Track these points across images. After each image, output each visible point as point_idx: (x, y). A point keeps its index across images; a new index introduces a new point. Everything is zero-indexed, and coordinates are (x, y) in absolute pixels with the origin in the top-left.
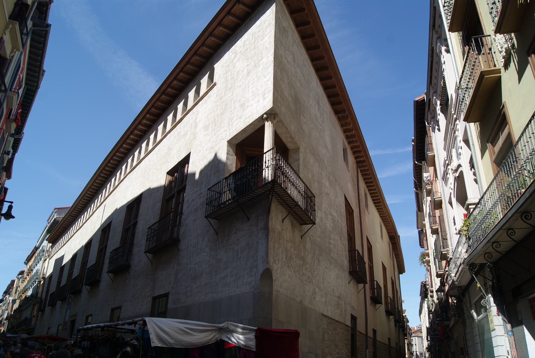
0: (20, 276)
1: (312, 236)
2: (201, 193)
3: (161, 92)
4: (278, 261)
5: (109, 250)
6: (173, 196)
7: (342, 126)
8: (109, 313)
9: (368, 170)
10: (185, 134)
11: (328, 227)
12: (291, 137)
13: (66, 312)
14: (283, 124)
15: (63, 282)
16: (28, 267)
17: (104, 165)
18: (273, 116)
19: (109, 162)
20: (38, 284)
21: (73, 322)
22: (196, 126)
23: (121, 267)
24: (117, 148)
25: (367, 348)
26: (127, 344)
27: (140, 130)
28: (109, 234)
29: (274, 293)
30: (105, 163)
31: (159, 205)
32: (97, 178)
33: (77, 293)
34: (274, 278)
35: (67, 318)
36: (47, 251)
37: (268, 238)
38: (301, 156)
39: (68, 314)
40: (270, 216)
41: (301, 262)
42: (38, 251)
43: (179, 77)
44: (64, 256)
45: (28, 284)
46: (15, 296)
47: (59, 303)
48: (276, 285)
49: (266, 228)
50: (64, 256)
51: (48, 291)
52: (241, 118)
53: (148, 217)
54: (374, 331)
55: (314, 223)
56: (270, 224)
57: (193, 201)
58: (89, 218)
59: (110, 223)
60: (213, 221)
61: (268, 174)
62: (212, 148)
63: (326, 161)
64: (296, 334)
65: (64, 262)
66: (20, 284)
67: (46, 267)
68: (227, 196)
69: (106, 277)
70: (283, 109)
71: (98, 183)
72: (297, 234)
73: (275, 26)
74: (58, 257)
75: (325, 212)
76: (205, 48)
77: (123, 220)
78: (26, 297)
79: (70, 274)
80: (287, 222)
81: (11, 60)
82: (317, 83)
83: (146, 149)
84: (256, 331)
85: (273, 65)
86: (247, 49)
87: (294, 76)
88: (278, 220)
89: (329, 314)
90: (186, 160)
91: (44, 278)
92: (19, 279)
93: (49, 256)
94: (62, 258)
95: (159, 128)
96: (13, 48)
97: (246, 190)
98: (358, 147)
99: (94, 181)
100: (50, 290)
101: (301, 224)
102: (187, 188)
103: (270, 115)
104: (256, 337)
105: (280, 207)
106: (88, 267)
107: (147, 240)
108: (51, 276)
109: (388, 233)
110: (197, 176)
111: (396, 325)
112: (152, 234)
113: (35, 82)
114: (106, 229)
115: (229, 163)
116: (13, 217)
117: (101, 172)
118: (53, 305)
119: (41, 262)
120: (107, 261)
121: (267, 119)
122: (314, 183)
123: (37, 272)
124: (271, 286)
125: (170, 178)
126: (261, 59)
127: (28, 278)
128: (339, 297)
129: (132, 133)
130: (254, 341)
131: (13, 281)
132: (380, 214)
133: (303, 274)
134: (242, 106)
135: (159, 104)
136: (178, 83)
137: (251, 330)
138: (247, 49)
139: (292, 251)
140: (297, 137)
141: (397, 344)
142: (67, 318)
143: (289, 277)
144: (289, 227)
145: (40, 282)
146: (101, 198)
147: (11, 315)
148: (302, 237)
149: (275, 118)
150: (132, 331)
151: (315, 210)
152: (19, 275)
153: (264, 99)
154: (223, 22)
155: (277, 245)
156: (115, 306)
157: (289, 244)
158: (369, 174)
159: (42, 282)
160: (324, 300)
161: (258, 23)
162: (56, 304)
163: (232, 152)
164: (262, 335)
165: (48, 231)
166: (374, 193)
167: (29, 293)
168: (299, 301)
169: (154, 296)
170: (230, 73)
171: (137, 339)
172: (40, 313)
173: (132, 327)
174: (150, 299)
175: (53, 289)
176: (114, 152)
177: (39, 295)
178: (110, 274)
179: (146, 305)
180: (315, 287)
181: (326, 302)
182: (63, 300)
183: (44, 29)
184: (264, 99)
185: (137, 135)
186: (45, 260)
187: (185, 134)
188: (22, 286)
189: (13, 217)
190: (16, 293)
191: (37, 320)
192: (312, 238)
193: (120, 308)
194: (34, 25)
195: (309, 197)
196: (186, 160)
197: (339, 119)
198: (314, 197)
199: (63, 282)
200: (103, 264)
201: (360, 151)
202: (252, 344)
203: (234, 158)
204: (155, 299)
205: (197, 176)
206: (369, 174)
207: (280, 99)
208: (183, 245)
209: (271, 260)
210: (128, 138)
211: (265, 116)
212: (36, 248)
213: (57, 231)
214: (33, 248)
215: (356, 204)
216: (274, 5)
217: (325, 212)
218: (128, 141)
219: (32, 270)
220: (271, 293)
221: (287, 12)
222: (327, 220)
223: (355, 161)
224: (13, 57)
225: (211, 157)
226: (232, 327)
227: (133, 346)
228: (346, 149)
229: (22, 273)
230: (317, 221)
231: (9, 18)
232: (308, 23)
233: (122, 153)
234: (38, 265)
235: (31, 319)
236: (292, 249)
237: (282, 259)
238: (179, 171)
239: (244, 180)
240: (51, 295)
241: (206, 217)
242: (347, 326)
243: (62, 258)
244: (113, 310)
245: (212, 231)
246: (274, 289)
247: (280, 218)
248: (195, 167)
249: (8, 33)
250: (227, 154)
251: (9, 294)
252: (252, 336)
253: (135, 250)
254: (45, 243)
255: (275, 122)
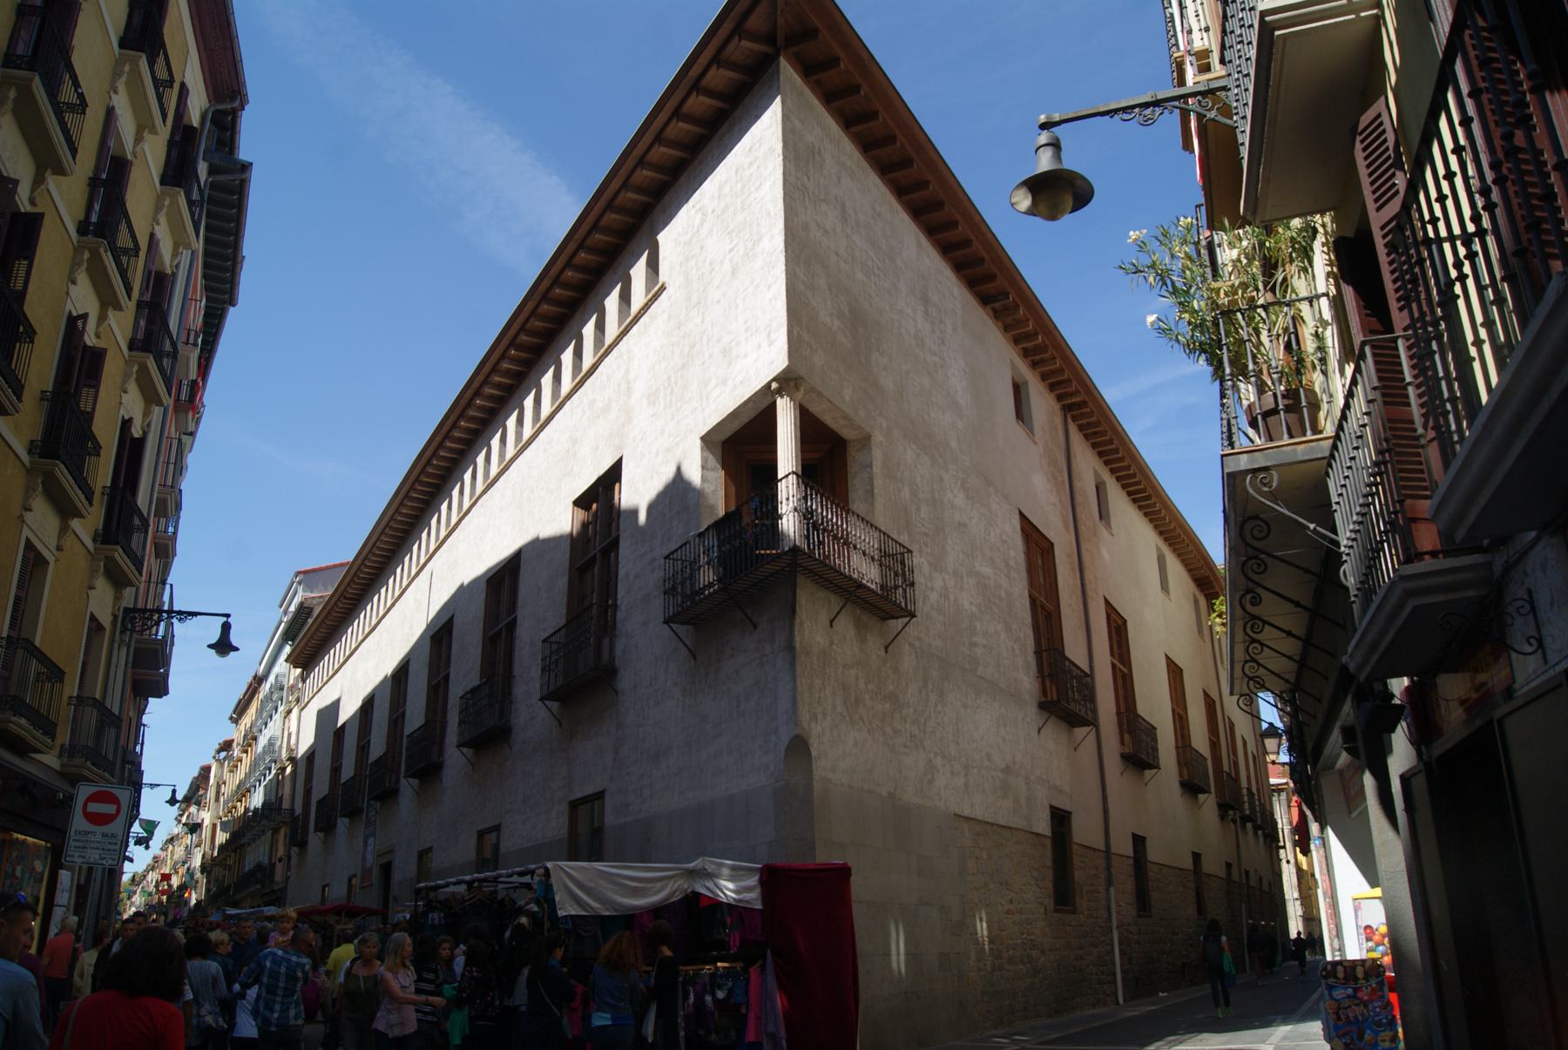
0: (223, 754)
1: (919, 639)
2: (653, 560)
3: (537, 296)
4: (824, 715)
5: (457, 690)
6: (592, 561)
7: (1006, 329)
8: (473, 842)
9: (1098, 423)
10: (607, 408)
11: (967, 606)
12: (846, 417)
13: (365, 843)
14: (820, 394)
15: (348, 772)
16: (242, 728)
17: (416, 472)
18: (792, 384)
19: (429, 463)
20: (277, 775)
21: (387, 869)
22: (629, 391)
23: (490, 735)
24: (445, 429)
25: (1109, 883)
26: (520, 911)
27: (498, 386)
28: (450, 647)
29: (817, 786)
30: (420, 466)
31: (563, 582)
32: (401, 504)
33: (388, 795)
34: (814, 753)
35: (370, 858)
36: (292, 688)
37: (794, 671)
38: (877, 454)
39: (370, 848)
40: (798, 621)
41: (887, 705)
42: (266, 688)
43: (576, 260)
44: (338, 701)
45: (248, 776)
46: (217, 808)
47: (342, 823)
48: (821, 769)
49: (790, 648)
50: (338, 701)
51: (308, 792)
52: (724, 382)
53: (541, 611)
54: (1139, 841)
55: (913, 615)
56: (797, 639)
57: (637, 576)
58: (393, 605)
59: (451, 619)
60: (682, 629)
61: (789, 523)
62: (668, 450)
63: (954, 444)
64: (843, 872)
65: (344, 715)
66: (226, 775)
67: (294, 729)
68: (707, 576)
69: (455, 758)
70: (819, 359)
71: (407, 515)
72: (874, 644)
73: (785, 159)
74: (323, 705)
75: (955, 573)
76: (630, 195)
77: (480, 614)
78: (247, 810)
79: (363, 748)
80: (845, 624)
81: (174, 274)
82: (919, 245)
83: (519, 434)
84: (761, 871)
85: (783, 259)
86: (727, 207)
87: (846, 262)
88: (817, 624)
89: (979, 813)
90: (613, 475)
91: (292, 759)
92: (221, 763)
93: (298, 700)
94: (335, 707)
95: (543, 381)
96: (176, 246)
97: (740, 560)
98: (1060, 371)
99: (397, 511)
100: (314, 791)
101: (884, 619)
102: (623, 544)
103: (786, 382)
104: (762, 882)
105: (822, 594)
106: (407, 731)
107: (543, 670)
108: (311, 755)
109: (1189, 571)
110: (642, 517)
111: (1222, 817)
112: (554, 657)
113: (225, 292)
114: (440, 635)
115: (709, 488)
116: (236, 649)
117: (411, 488)
118: (327, 827)
119: (278, 717)
120: (453, 718)
121: (779, 392)
122: (918, 509)
123: (271, 743)
124: (810, 771)
125: (581, 515)
126: (760, 240)
127: (247, 760)
128: (1007, 770)
129: (477, 393)
130: (758, 890)
131: (206, 770)
132: (1156, 527)
133: (896, 731)
134: (726, 352)
135: (537, 324)
136: (578, 276)
137: (750, 870)
138: (727, 207)
139: (862, 684)
140: (862, 413)
141: (1229, 865)
142: (370, 858)
143: (856, 745)
144: (851, 632)
145: (283, 769)
146: (418, 551)
147: (213, 859)
148: (886, 648)
149: (797, 388)
150: (528, 886)
151: (912, 584)
152: (219, 751)
153: (771, 344)
154: (665, 135)
155: (818, 682)
156: (487, 825)
157: (853, 672)
158: (1104, 433)
159: (289, 770)
160: (960, 781)
161: (747, 140)
162: (335, 825)
163: (713, 462)
164: (772, 878)
165: (289, 635)
166: (1128, 477)
167: (257, 799)
168: (884, 794)
169: (573, 798)
170: (693, 262)
171: (538, 902)
172: (295, 849)
173: (527, 879)
174: (564, 807)
175: (321, 788)
176: (438, 439)
177: (286, 805)
178: (465, 750)
179: (555, 825)
180: (932, 756)
181: (966, 785)
182: (353, 813)
183: (237, 176)
184: (771, 344)
185: (491, 398)
186: (289, 712)
187: (607, 408)
188: (233, 781)
189: (236, 649)
190: (217, 800)
191: (289, 868)
192: (917, 644)
193: (497, 828)
194: (211, 172)
195: (895, 559)
196: (613, 475)
197: (997, 315)
198: (910, 551)
199: (348, 772)
200: (444, 724)
201: (1068, 381)
202: (754, 898)
203: (719, 475)
204: (574, 805)
205: (642, 517)
206: (1104, 433)
207: (806, 337)
208: (624, 681)
209: (805, 716)
210: (469, 404)
211: (774, 385)
212: (259, 680)
213: (314, 635)
214: (249, 679)
215: (1065, 522)
216: (778, 100)
217: (955, 573)
218: (471, 413)
219: (255, 739)
220: (809, 786)
221: (815, 102)
222: (962, 589)
223: (1056, 406)
224: (177, 266)
225: (668, 474)
226: (711, 868)
227: (531, 915)
228: (1026, 383)
229: (227, 746)
230: (922, 608)
231: (162, 183)
232: (874, 115)
233: (460, 440)
234: (270, 725)
235: (273, 866)
236: (861, 682)
237: (835, 707)
238: (600, 495)
239: (737, 543)
240: (319, 802)
241: (666, 622)
242: (1037, 835)
243: (335, 707)
244: (481, 834)
245: (684, 651)
246: (816, 777)
247: (824, 618)
248: (636, 494)
249: (163, 219)
250: (703, 468)
251: (198, 804)
252: (753, 881)
253: (519, 690)
254: (281, 666)
255: (799, 395)
